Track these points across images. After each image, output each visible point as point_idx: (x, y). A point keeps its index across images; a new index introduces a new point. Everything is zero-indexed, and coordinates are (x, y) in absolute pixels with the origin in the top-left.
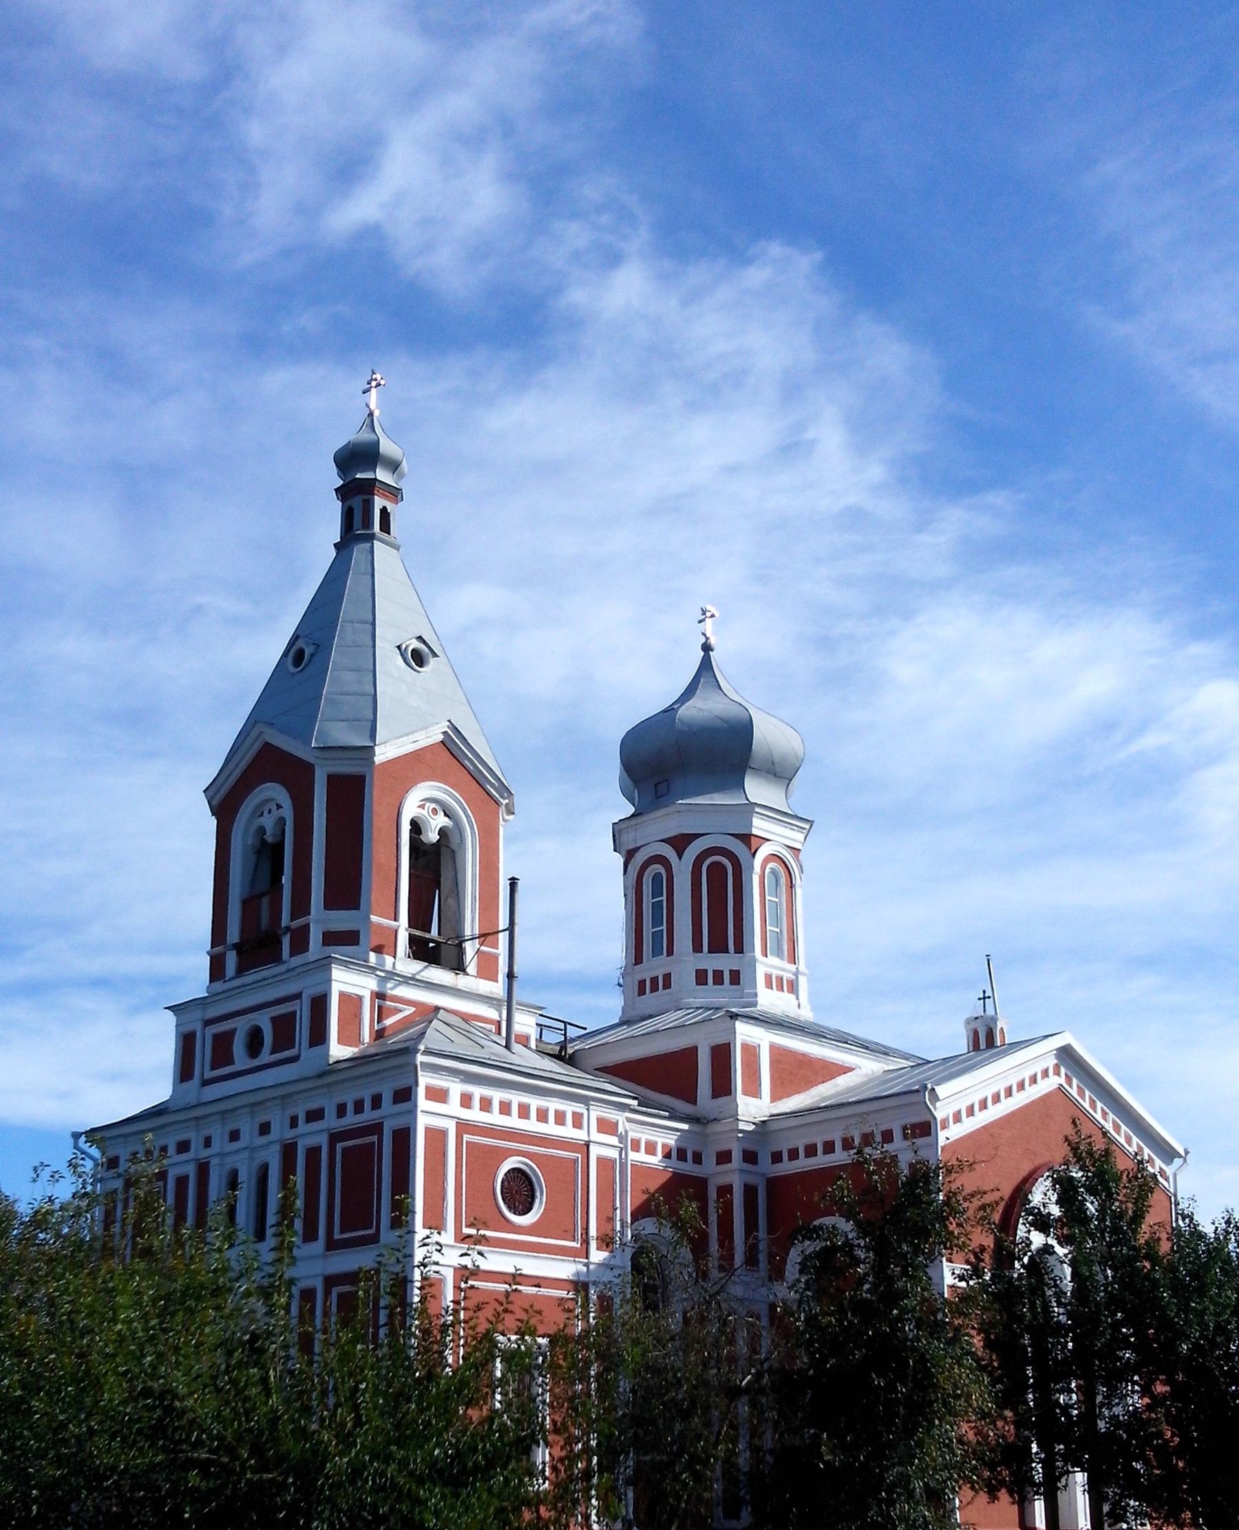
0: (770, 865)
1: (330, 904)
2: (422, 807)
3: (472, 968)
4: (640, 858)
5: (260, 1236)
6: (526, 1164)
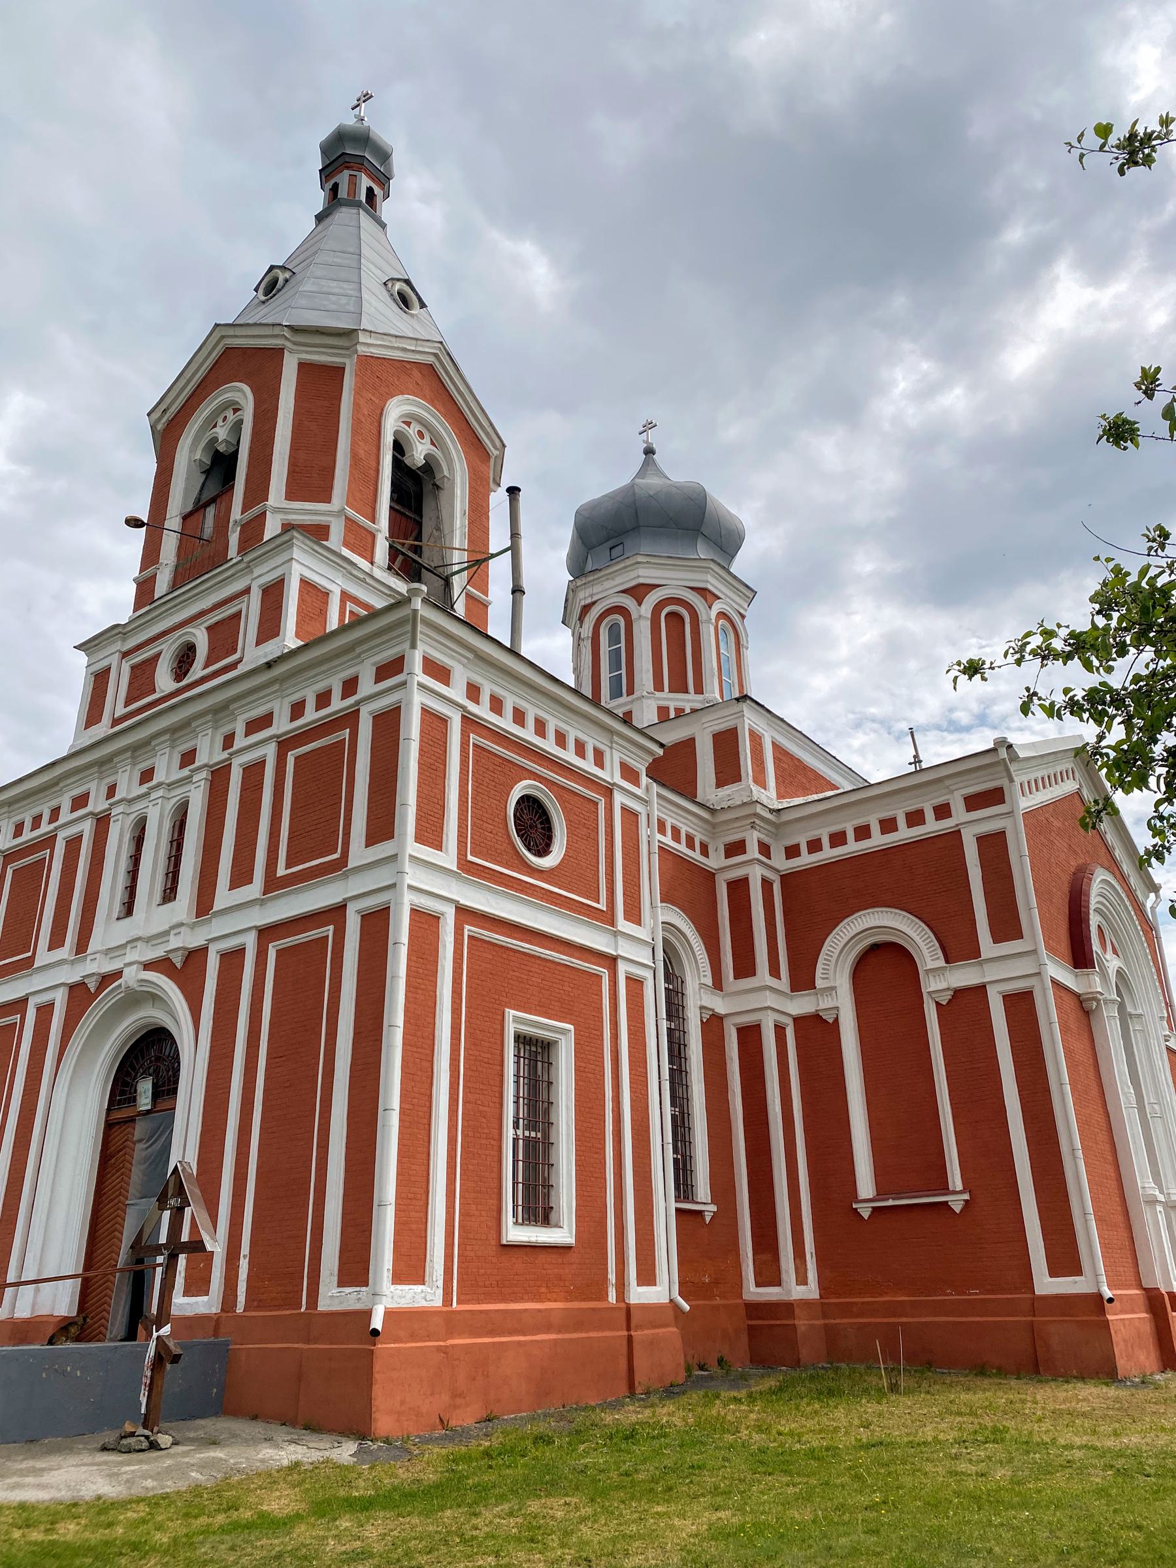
0: (721, 622)
2: (408, 424)
4: (595, 612)
5: (170, 894)
6: (537, 788)
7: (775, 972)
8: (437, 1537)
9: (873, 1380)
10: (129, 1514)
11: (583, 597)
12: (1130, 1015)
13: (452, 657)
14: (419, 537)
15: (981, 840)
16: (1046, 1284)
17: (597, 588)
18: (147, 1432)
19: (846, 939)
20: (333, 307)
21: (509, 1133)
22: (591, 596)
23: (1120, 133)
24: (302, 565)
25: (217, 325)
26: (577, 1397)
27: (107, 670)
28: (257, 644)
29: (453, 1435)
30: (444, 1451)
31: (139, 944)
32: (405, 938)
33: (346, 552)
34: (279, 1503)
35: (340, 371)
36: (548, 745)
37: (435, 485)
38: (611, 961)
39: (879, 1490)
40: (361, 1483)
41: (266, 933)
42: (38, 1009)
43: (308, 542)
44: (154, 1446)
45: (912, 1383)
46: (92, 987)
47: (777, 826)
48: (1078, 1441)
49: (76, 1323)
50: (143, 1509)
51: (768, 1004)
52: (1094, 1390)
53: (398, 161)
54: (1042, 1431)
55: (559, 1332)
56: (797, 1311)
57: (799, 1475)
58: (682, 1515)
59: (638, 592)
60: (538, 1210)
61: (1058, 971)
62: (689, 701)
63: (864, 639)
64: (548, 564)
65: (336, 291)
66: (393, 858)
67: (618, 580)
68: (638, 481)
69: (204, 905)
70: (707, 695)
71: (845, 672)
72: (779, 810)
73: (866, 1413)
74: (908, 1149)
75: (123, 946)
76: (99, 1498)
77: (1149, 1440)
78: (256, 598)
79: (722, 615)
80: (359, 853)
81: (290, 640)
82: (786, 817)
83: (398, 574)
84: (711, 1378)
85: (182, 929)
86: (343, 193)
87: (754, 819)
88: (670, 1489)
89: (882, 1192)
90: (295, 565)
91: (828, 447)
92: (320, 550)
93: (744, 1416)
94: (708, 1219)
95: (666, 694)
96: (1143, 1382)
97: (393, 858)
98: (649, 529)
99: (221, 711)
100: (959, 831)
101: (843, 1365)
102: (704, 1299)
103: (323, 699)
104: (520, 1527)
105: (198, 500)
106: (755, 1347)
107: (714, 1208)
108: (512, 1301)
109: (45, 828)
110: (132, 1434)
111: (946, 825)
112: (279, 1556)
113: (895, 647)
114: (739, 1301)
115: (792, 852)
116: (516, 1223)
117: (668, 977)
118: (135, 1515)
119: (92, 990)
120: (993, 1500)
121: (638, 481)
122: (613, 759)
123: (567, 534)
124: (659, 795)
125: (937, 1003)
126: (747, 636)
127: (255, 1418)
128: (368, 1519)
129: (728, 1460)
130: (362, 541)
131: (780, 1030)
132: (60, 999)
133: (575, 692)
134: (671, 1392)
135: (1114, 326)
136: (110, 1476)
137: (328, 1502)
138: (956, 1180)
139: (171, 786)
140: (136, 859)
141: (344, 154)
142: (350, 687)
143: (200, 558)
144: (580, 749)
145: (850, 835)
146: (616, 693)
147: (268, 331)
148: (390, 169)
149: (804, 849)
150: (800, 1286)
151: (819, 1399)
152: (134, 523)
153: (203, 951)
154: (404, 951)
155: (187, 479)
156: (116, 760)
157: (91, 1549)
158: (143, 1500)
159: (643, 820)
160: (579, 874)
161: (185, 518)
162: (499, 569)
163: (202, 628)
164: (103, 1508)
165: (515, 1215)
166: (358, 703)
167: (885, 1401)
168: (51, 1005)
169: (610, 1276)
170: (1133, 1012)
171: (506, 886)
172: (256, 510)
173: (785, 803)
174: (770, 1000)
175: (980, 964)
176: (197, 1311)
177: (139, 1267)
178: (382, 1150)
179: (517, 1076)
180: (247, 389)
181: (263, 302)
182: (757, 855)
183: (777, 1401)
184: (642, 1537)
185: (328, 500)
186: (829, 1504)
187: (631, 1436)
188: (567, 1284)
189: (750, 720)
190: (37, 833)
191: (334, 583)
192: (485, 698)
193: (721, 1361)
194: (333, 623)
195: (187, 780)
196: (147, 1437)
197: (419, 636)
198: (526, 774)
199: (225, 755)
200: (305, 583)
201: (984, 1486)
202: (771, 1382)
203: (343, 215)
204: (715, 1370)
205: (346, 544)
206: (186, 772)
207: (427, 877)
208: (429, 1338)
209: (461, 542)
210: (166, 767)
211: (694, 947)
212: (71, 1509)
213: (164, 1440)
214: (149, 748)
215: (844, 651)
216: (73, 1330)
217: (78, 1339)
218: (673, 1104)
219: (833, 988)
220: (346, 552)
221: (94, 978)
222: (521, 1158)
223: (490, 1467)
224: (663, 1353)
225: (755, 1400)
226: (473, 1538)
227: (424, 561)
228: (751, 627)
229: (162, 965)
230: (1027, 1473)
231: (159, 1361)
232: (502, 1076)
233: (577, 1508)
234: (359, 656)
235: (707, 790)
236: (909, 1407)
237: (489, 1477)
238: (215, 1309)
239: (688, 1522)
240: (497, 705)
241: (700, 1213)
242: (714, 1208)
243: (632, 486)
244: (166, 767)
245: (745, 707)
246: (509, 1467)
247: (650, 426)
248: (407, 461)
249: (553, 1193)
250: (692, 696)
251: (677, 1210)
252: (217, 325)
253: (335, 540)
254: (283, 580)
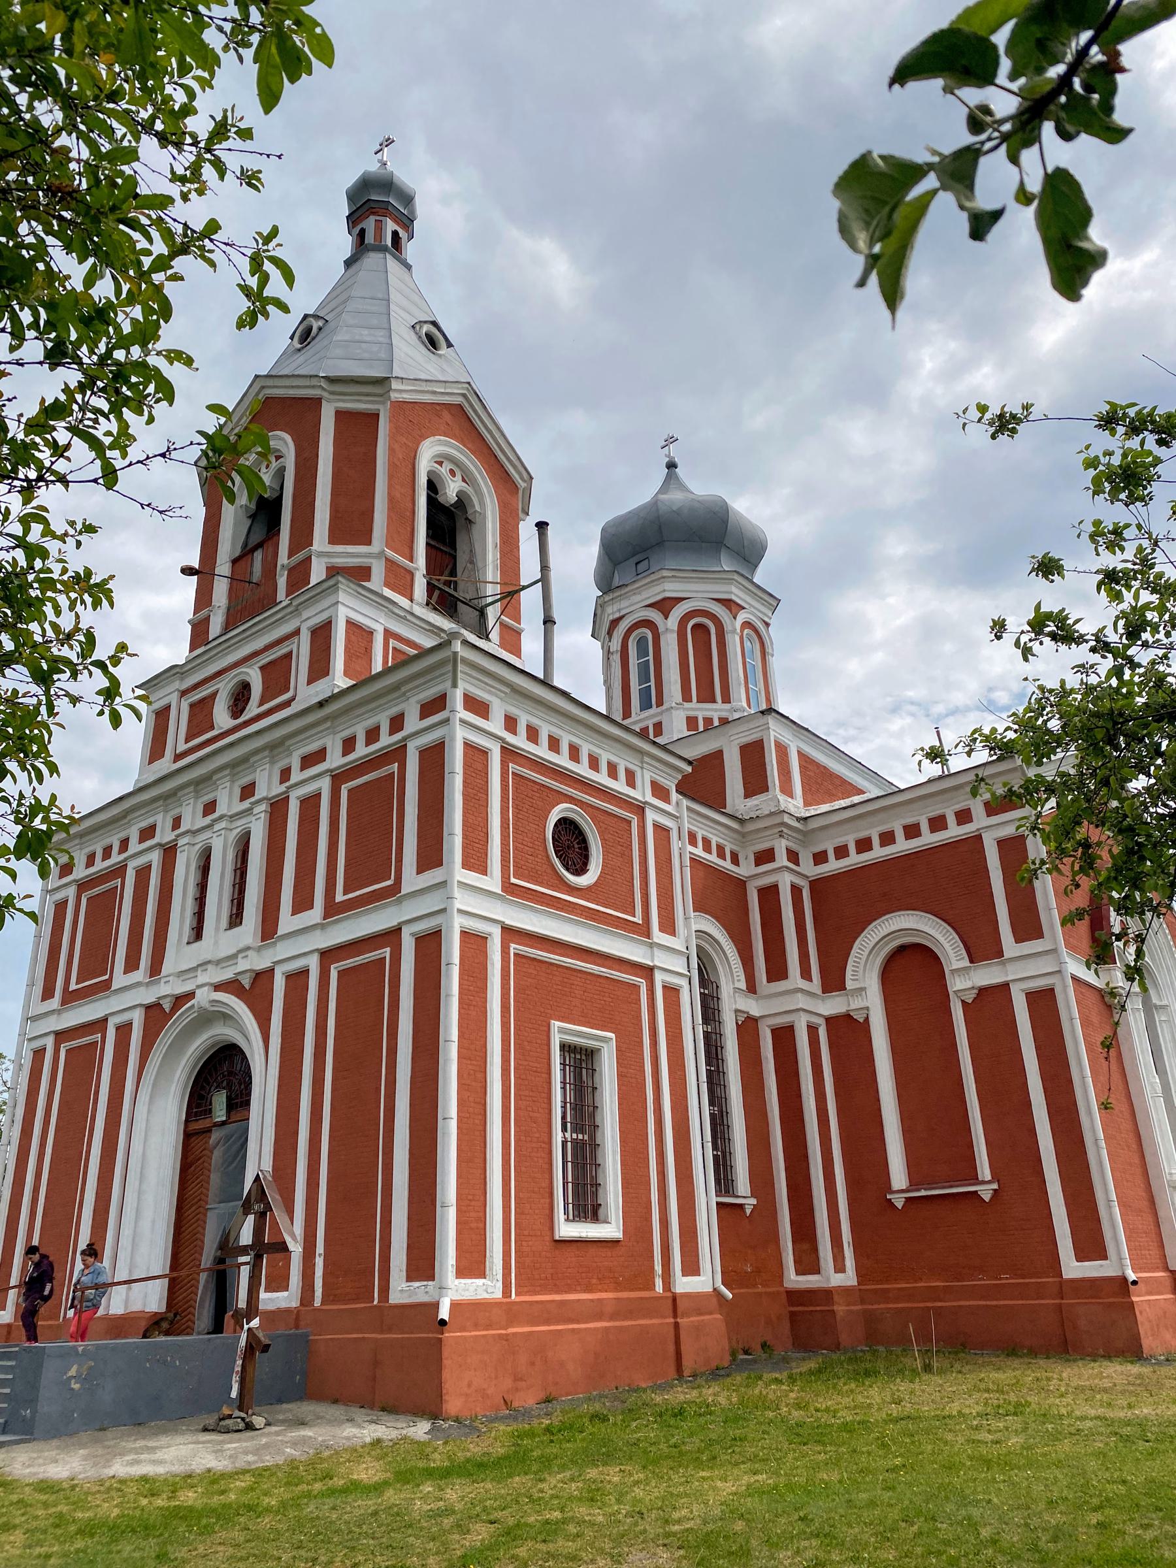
0: (746, 631)
1: (335, 538)
2: (440, 463)
3: (495, 635)
5: (236, 919)
7: (806, 974)
8: (509, 1498)
9: (907, 1361)
10: (238, 1483)
11: (612, 612)
12: (1156, 1007)
13: (490, 692)
14: (453, 573)
15: (1001, 843)
16: (1073, 1268)
17: (624, 604)
18: (243, 1415)
19: (874, 941)
20: (366, 355)
21: (558, 1136)
22: (619, 610)
23: (994, 410)
24: (347, 608)
25: (257, 376)
26: (631, 1376)
27: (168, 708)
28: (309, 683)
29: (516, 1414)
30: (509, 1429)
31: (209, 967)
32: (456, 959)
33: (387, 592)
34: (367, 1472)
35: (376, 416)
36: (582, 769)
37: (467, 519)
38: (648, 972)
39: (901, 1455)
40: (436, 1456)
41: (328, 955)
42: (118, 1029)
43: (351, 585)
44: (249, 1427)
45: (946, 1364)
46: (167, 1007)
47: (805, 834)
48: (1093, 1413)
49: (166, 1319)
50: (249, 1480)
51: (800, 1006)
52: (1119, 1368)
53: (421, 207)
54: (1061, 1405)
55: (611, 1319)
56: (836, 1298)
57: (831, 1444)
58: (724, 1479)
59: (664, 606)
60: (587, 1206)
61: (1076, 967)
62: (716, 710)
63: (900, 622)
64: (577, 561)
65: (368, 339)
66: (443, 884)
67: (645, 595)
68: (661, 497)
69: (269, 929)
70: (734, 704)
71: (879, 657)
72: (806, 818)
73: (898, 1390)
74: (938, 1137)
75: (194, 969)
76: (209, 1470)
77: (1159, 1411)
78: (305, 637)
79: (747, 624)
80: (411, 880)
81: (339, 680)
82: (813, 824)
83: (435, 609)
84: (755, 1361)
85: (249, 953)
86: (370, 238)
87: (782, 830)
88: (715, 1458)
89: (915, 1181)
90: (341, 608)
91: (857, 432)
92: (363, 592)
93: (783, 1394)
94: (748, 1212)
95: (694, 704)
96: (1167, 1360)
97: (443, 884)
98: (673, 545)
99: (275, 748)
100: (980, 835)
101: (881, 1348)
102: (747, 1287)
103: (372, 735)
104: (581, 1490)
105: (245, 544)
106: (792, 1332)
107: (754, 1201)
108: (566, 1292)
109: (116, 858)
110: (230, 1417)
111: (968, 829)
112: (375, 1513)
113: (930, 630)
114: (782, 1289)
115: (820, 858)
116: (567, 1220)
117: (703, 982)
118: (243, 1484)
119: (167, 1010)
120: (1006, 1463)
121: (661, 497)
122: (644, 778)
123: (593, 550)
124: (688, 808)
125: (963, 1001)
126: (772, 643)
127: (336, 1401)
128: (447, 1485)
129: (768, 1433)
130: (400, 580)
131: (812, 1030)
132: (137, 1018)
133: (607, 718)
134: (716, 1374)
135: (1147, 295)
136: (216, 1452)
137: (411, 1471)
138: (985, 1172)
139: (233, 817)
140: (203, 887)
141: (369, 200)
142: (397, 723)
143: (250, 601)
144: (613, 771)
145: (876, 841)
146: (646, 705)
147: (307, 382)
148: (413, 212)
149: (831, 855)
150: (838, 1275)
151: (856, 1380)
152: (188, 571)
153: (270, 972)
154: (455, 971)
155: (235, 524)
156: (180, 794)
157: (213, 1510)
158: (248, 1471)
159: (674, 835)
160: (616, 891)
161: (235, 562)
162: (530, 600)
163: (256, 667)
164: (213, 1479)
165: (566, 1212)
166: (405, 739)
167: (917, 1380)
168: (129, 1025)
169: (656, 1268)
170: (1158, 1003)
171: (548, 905)
172: (300, 556)
173: (812, 811)
174: (801, 1002)
175: (1003, 963)
176: (279, 1306)
177: (221, 1267)
178: (443, 1151)
179: (564, 1083)
180: (288, 438)
181: (299, 350)
182: (786, 863)
183: (816, 1381)
184: (687, 1495)
185: (369, 542)
186: (855, 1467)
187: (680, 1413)
188: (616, 1275)
189: (775, 732)
190: (108, 863)
191: (377, 622)
192: (522, 728)
193: (764, 1346)
194: (377, 667)
195: (248, 812)
196: (243, 1419)
197: (459, 675)
198: (562, 797)
199: (283, 788)
200: (350, 623)
201: (995, 1450)
202: (813, 1365)
203: (372, 260)
204: (759, 1352)
205: (387, 584)
206: (246, 804)
207: (474, 900)
208: (488, 1327)
209: (494, 576)
210: (227, 800)
211: (728, 953)
212: (188, 1479)
213: (258, 1421)
214: (210, 782)
215: (879, 634)
216: (165, 1325)
217: (167, 1333)
218: (711, 1103)
219: (863, 989)
220: (387, 592)
221: (168, 999)
222: (570, 1179)
223: (552, 1441)
224: (708, 1338)
225: (795, 1381)
226: (540, 1499)
227: (460, 594)
228: (776, 634)
229: (231, 986)
230: (1037, 1440)
231: (250, 1349)
232: (550, 1083)
233: (631, 1475)
234: (404, 694)
235: (737, 801)
236: (941, 1385)
237: (554, 1449)
238: (295, 1304)
239: (729, 1484)
240: (533, 734)
241: (741, 1207)
242: (754, 1201)
243: (655, 502)
244: (227, 800)
245: (771, 720)
246: (569, 1441)
247: (671, 440)
248: (441, 499)
249: (600, 1191)
250: (719, 705)
251: (718, 1203)
252: (257, 376)
253: (376, 582)
254: (330, 622)
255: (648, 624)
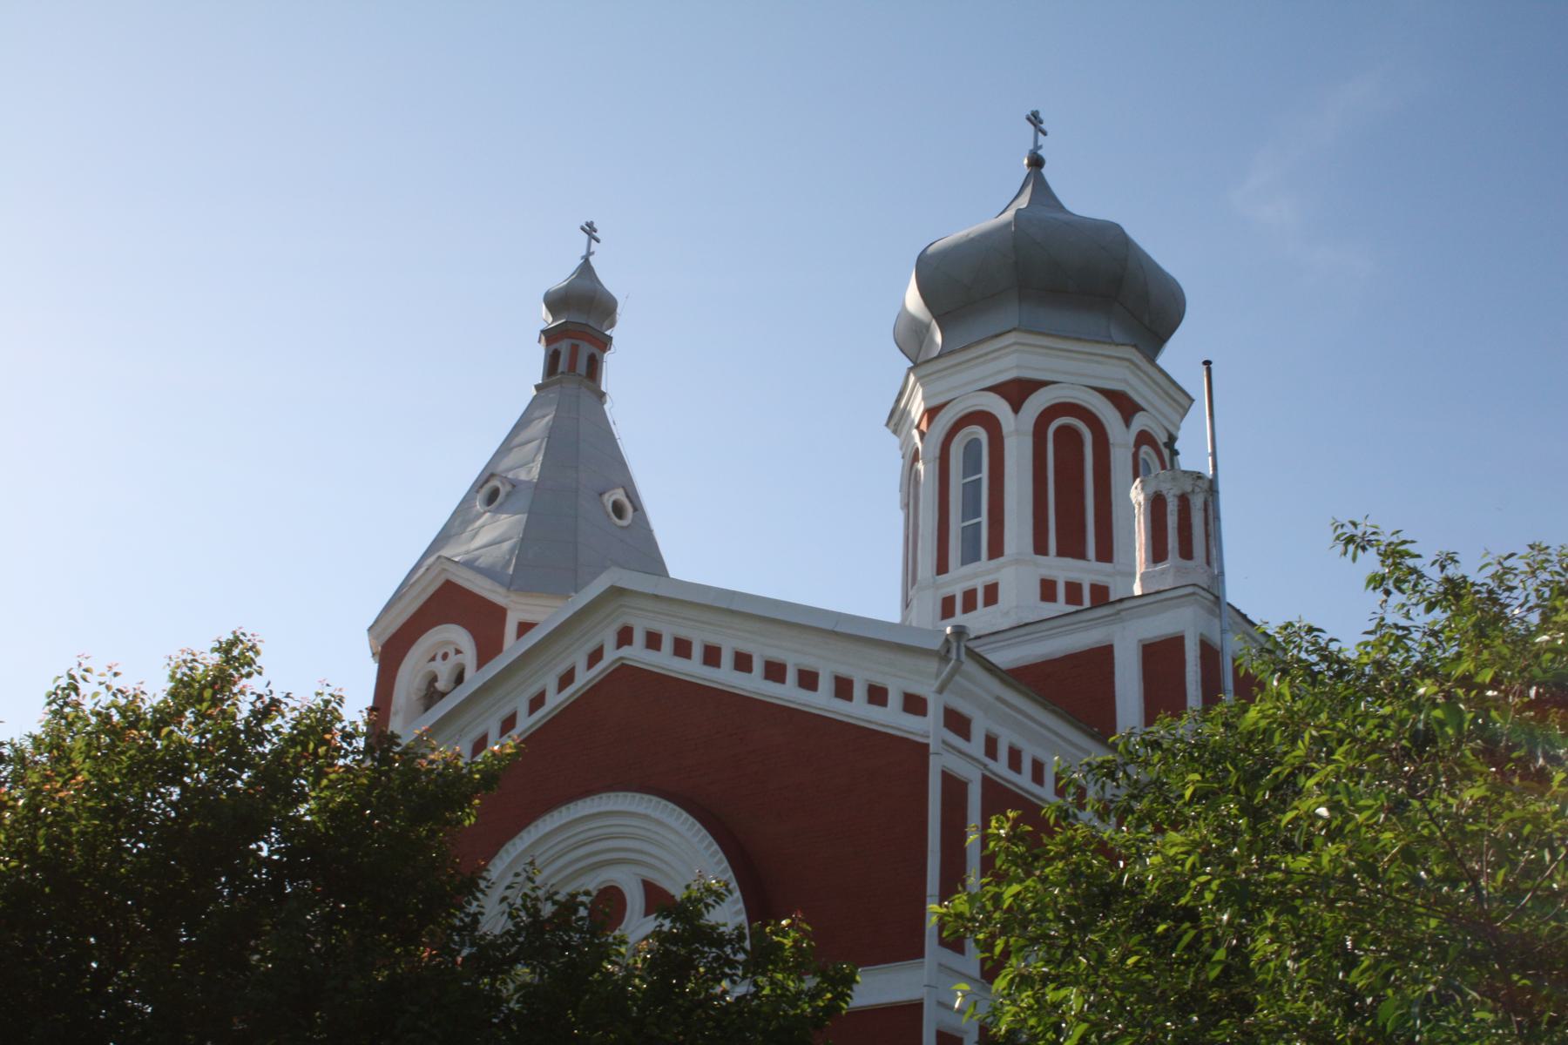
234: (1118, 612)
255: (988, 421)
